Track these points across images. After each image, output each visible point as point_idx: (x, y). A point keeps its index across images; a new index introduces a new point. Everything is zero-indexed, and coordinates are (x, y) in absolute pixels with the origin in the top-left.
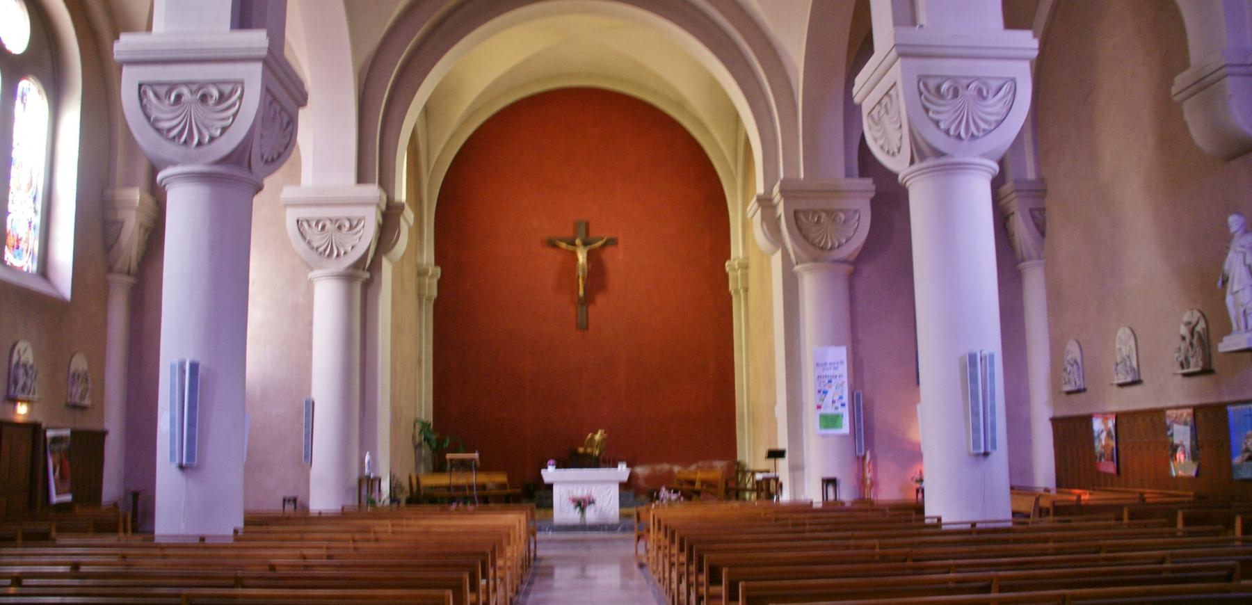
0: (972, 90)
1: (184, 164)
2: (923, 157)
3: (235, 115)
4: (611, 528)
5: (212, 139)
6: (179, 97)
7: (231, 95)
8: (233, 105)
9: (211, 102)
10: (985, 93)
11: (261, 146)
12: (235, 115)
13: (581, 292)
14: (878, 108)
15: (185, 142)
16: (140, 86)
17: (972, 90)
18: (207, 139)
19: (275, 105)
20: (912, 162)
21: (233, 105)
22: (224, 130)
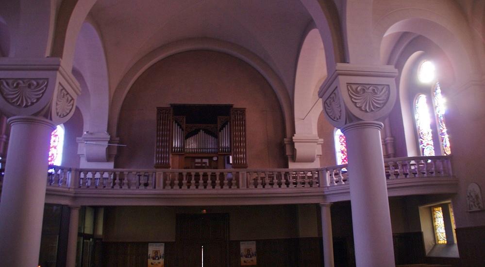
0: (370, 90)
1: (19, 115)
2: (351, 121)
3: (43, 93)
4: (241, 241)
5: (32, 104)
6: (18, 84)
7: (42, 84)
8: (42, 89)
9: (32, 87)
10: (376, 91)
11: (57, 109)
12: (43, 93)
13: (231, 157)
14: (330, 99)
15: (19, 105)
16: (388, 85)
17: (370, 90)
18: (30, 104)
19: (63, 91)
20: (346, 123)
21: (42, 89)
22: (38, 99)
